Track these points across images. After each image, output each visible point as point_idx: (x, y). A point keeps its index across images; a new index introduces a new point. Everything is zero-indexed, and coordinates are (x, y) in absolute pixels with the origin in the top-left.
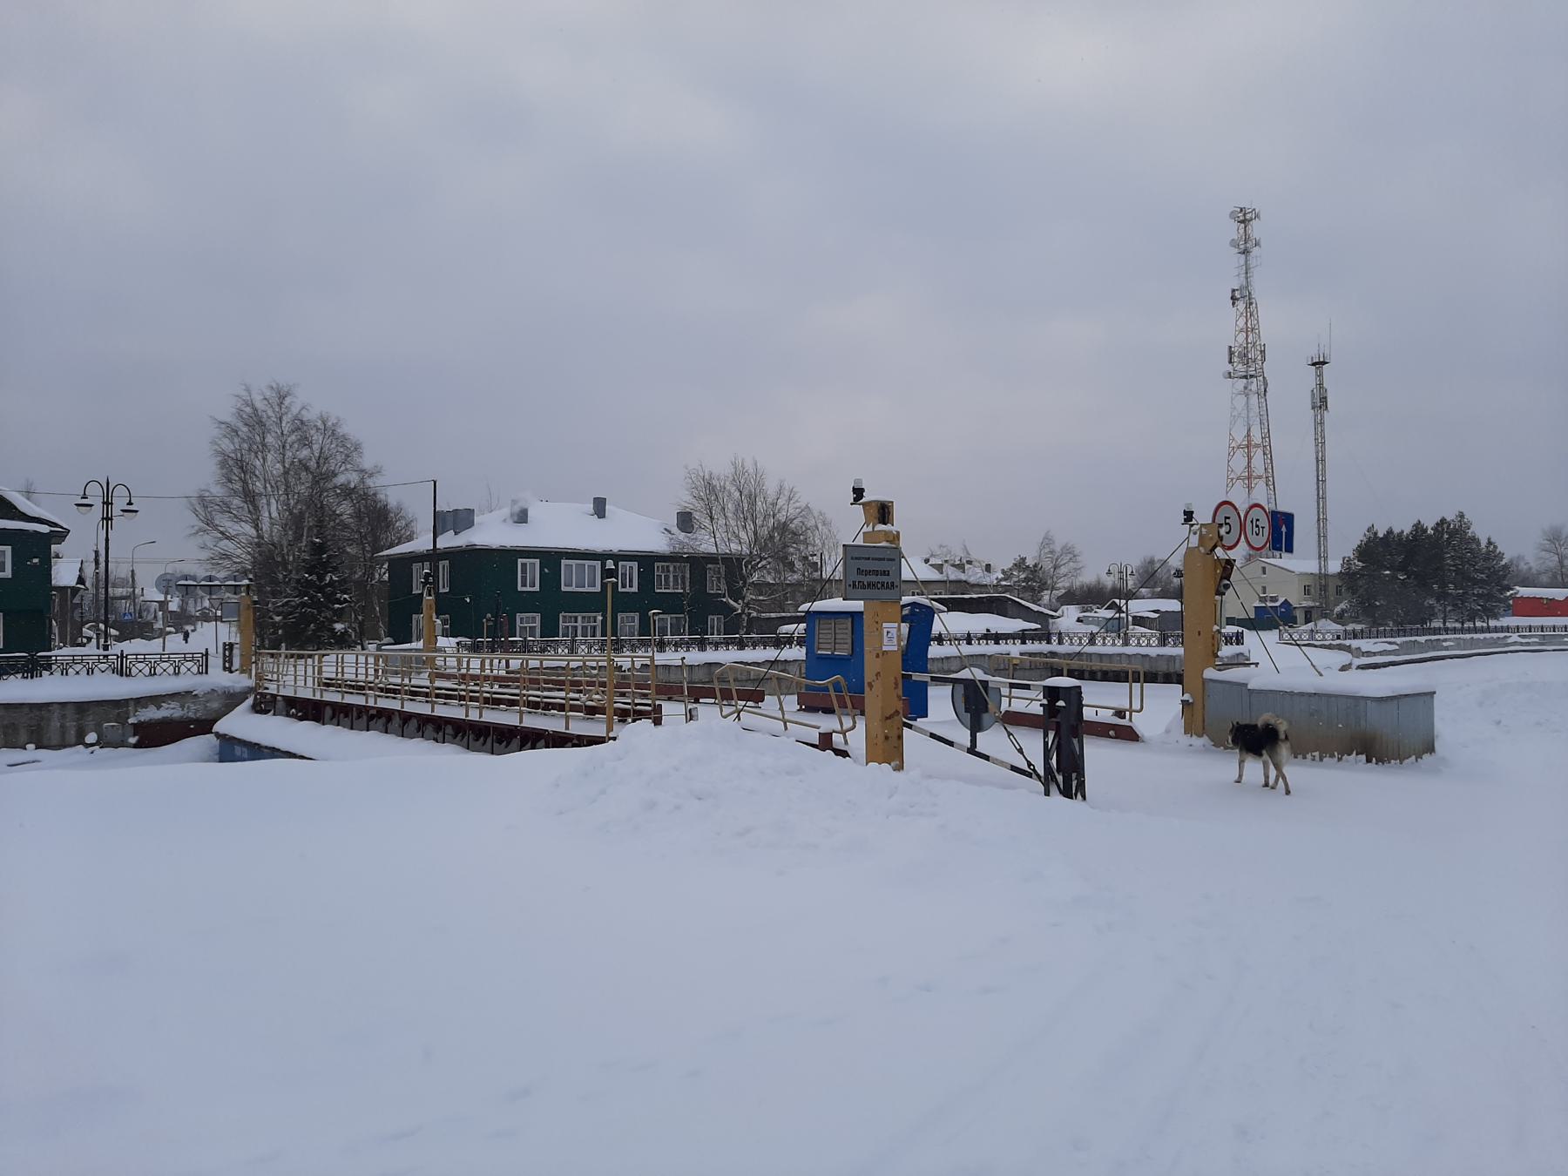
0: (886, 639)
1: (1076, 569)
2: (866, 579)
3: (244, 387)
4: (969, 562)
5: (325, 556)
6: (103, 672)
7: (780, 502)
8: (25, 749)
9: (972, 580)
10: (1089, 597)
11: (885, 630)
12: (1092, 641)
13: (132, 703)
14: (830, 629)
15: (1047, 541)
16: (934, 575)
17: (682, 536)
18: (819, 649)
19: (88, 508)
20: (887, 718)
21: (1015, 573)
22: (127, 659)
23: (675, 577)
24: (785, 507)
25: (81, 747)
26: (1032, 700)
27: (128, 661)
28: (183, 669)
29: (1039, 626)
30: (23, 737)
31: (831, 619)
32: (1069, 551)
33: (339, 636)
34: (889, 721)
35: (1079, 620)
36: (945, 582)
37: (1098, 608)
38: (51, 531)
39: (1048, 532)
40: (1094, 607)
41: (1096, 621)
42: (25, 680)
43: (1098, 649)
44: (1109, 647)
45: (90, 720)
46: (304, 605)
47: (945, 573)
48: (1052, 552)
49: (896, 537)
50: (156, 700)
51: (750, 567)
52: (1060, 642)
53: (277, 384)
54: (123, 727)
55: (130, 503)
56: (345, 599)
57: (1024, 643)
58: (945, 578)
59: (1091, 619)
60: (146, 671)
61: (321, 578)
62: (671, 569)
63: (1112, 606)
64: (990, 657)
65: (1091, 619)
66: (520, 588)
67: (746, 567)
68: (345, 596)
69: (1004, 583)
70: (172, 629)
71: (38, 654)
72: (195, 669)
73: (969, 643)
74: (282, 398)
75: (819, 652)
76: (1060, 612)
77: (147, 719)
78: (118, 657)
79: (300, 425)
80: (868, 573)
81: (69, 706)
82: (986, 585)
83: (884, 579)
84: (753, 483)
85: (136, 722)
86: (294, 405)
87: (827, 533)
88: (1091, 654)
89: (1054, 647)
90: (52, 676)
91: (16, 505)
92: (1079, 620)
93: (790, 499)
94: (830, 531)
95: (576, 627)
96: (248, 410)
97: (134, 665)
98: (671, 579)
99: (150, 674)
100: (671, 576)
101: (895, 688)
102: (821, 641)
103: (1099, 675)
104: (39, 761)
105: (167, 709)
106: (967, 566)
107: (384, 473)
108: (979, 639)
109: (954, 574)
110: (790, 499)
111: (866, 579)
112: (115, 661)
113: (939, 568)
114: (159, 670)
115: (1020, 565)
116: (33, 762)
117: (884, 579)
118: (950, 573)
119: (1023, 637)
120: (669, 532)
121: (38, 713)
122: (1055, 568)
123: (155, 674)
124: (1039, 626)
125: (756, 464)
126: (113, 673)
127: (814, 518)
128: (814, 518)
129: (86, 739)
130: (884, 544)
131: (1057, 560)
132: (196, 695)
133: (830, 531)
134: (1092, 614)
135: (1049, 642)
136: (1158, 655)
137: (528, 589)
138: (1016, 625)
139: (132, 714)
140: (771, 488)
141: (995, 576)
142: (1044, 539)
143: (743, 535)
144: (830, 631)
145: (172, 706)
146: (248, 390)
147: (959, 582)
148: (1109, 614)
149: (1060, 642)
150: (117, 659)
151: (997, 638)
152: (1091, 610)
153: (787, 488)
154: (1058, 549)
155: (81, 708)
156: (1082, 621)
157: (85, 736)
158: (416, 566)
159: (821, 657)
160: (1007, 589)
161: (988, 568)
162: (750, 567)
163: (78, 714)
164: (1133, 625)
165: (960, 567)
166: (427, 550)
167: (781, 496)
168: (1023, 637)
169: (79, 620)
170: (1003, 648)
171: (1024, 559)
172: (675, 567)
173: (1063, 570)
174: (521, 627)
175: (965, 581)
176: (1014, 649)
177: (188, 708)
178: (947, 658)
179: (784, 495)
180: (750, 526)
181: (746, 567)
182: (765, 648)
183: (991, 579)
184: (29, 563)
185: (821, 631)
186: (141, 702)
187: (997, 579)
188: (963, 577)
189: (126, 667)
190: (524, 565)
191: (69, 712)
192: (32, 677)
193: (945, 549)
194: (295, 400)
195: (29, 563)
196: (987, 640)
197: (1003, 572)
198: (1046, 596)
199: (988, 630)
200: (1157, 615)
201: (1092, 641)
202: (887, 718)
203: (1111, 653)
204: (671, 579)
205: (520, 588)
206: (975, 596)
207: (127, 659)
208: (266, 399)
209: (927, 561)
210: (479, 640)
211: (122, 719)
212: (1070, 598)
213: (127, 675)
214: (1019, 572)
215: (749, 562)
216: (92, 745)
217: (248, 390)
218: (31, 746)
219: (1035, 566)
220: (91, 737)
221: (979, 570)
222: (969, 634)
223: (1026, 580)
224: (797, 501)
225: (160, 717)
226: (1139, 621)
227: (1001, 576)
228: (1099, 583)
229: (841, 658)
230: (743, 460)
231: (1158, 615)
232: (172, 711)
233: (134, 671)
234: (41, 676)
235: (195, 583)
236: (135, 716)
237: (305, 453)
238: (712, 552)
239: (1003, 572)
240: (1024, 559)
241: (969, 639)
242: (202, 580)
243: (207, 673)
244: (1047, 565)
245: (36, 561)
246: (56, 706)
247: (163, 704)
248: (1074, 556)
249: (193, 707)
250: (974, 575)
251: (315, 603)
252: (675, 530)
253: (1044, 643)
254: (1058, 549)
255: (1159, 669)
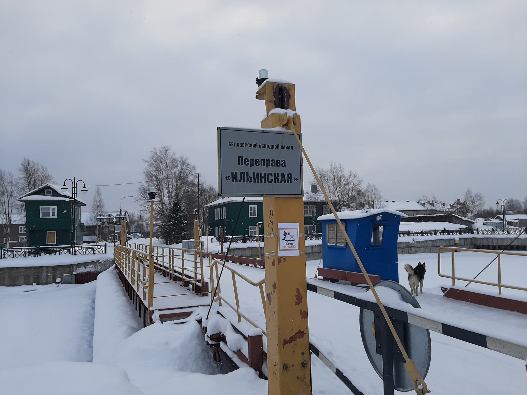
0: (282, 243)
1: (482, 203)
2: (251, 170)
3: (154, 148)
4: (436, 202)
5: (178, 207)
6: (65, 253)
7: (351, 179)
8: (32, 285)
9: (438, 209)
10: (488, 215)
11: (282, 233)
12: (493, 233)
13: (75, 266)
14: (334, 230)
15: (468, 192)
16: (421, 208)
17: (312, 194)
18: (329, 242)
19: (86, 191)
20: (286, 342)
21: (455, 206)
22: (75, 248)
23: (310, 210)
24: (353, 181)
25: (54, 284)
26: (471, 281)
27: (75, 249)
28: (97, 252)
29: (467, 227)
30: (32, 280)
31: (334, 224)
32: (477, 196)
33: (182, 236)
34: (288, 345)
35: (484, 224)
36: (426, 210)
37: (492, 219)
38: (70, 200)
39: (469, 189)
40: (490, 218)
41: (491, 224)
42: (35, 257)
43: (496, 236)
44: (500, 235)
45: (58, 273)
46: (170, 225)
47: (426, 207)
48: (471, 197)
49: (295, 121)
50: (84, 264)
51: (339, 205)
52: (478, 233)
53: (164, 146)
54: (71, 275)
55: (84, 187)
56: (186, 222)
57: (461, 234)
58: (426, 209)
59: (489, 223)
60: (82, 253)
61: (177, 215)
62: (308, 208)
63: (498, 218)
64: (445, 240)
65: (489, 223)
66: (250, 216)
67: (338, 205)
68: (186, 221)
69: (451, 210)
70: (140, 235)
71: (40, 247)
72: (101, 252)
73: (423, 235)
74: (166, 151)
75: (329, 244)
76: (475, 221)
77: (81, 272)
78: (104, 246)
79: (174, 162)
80: (253, 162)
81: (49, 268)
82: (443, 211)
83: (280, 170)
84: (339, 172)
85: (76, 274)
86: (170, 153)
87: (377, 193)
88: (493, 238)
89: (475, 235)
90: (45, 255)
91: (57, 191)
92: (484, 224)
93: (355, 177)
94: (377, 192)
95: (256, 231)
96: (155, 156)
97: (87, 250)
98: (308, 211)
99: (84, 254)
100: (308, 210)
101: (297, 303)
102: (330, 237)
103: (497, 247)
104: (37, 290)
105: (89, 268)
106: (435, 204)
107: (202, 176)
108: (440, 233)
109: (429, 207)
110: (355, 177)
111: (251, 170)
112: (103, 247)
113: (423, 205)
114: (87, 252)
115: (458, 202)
116: (35, 290)
117: (280, 170)
118: (428, 207)
119: (460, 231)
120: (308, 193)
121: (38, 270)
122: (473, 203)
123: (86, 254)
124: (467, 227)
125: (340, 165)
126: (69, 254)
127: (371, 187)
128: (371, 187)
129: (56, 280)
130: (278, 129)
131: (473, 200)
132: (101, 262)
133: (377, 192)
134: (490, 221)
135: (472, 233)
136: (525, 238)
137: (253, 217)
138: (457, 226)
139: (74, 270)
140: (346, 174)
141: (447, 207)
142: (467, 191)
143: (336, 193)
144: (334, 232)
145: (91, 267)
146: (155, 149)
147: (432, 210)
148: (498, 221)
149: (478, 233)
150: (104, 247)
151: (448, 232)
152: (489, 220)
153: (353, 173)
154: (473, 195)
155: (55, 268)
156: (485, 224)
157: (56, 280)
158: (216, 210)
159: (331, 248)
160: (452, 212)
161: (444, 204)
162: (339, 205)
163: (54, 270)
164: (508, 225)
165: (433, 205)
166: (219, 204)
167: (351, 177)
168: (460, 231)
169: (105, 232)
170: (451, 236)
171: (459, 200)
172: (310, 207)
173: (476, 204)
174: (251, 231)
175: (434, 210)
176: (457, 237)
177: (98, 267)
178: (426, 241)
179: (352, 176)
180: (338, 189)
181: (338, 205)
182: (311, 240)
183: (446, 208)
184: (63, 212)
185: (329, 232)
186: (78, 265)
187: (448, 208)
188: (433, 208)
189: (74, 252)
190: (251, 208)
191: (50, 270)
192: (37, 256)
193: (425, 198)
194: (170, 151)
195: (63, 212)
196: (444, 233)
197: (450, 205)
198: (469, 215)
199: (444, 229)
200: (518, 221)
201: (493, 233)
202: (286, 342)
203: (502, 238)
204: (308, 211)
205: (250, 216)
206: (438, 215)
207: (75, 248)
208: (161, 152)
209: (418, 202)
210: (246, 236)
211: (71, 272)
212: (479, 215)
213: (74, 255)
214: (457, 205)
215: (339, 204)
216: (59, 283)
217: (155, 149)
218: (34, 284)
219: (464, 202)
220: (58, 280)
221: (440, 205)
222: (435, 231)
223: (460, 208)
224: (357, 178)
225: (86, 271)
226: (510, 223)
227: (449, 207)
228: (491, 209)
229: (340, 248)
230: (334, 163)
231: (519, 221)
232: (91, 269)
233: (77, 253)
234: (41, 255)
235: (104, 217)
236: (76, 271)
237: (176, 170)
238: (324, 200)
239: (450, 205)
240: (459, 200)
241: (435, 233)
242: (107, 216)
243: (106, 253)
244: (469, 204)
245: (65, 211)
246: (45, 268)
247: (87, 266)
248: (481, 198)
249: (99, 267)
250: (438, 207)
251: (174, 225)
252: (310, 192)
253: (470, 233)
254: (473, 195)
255: (526, 245)
